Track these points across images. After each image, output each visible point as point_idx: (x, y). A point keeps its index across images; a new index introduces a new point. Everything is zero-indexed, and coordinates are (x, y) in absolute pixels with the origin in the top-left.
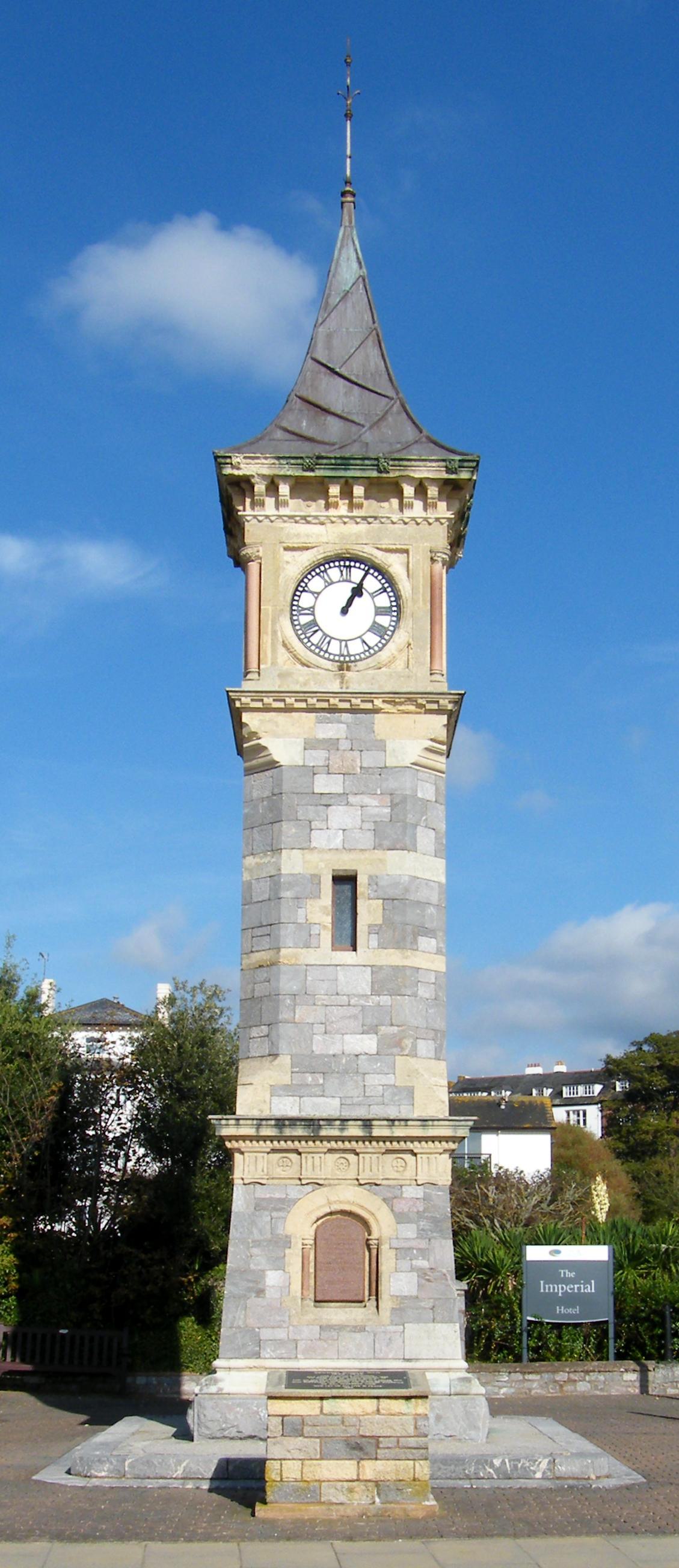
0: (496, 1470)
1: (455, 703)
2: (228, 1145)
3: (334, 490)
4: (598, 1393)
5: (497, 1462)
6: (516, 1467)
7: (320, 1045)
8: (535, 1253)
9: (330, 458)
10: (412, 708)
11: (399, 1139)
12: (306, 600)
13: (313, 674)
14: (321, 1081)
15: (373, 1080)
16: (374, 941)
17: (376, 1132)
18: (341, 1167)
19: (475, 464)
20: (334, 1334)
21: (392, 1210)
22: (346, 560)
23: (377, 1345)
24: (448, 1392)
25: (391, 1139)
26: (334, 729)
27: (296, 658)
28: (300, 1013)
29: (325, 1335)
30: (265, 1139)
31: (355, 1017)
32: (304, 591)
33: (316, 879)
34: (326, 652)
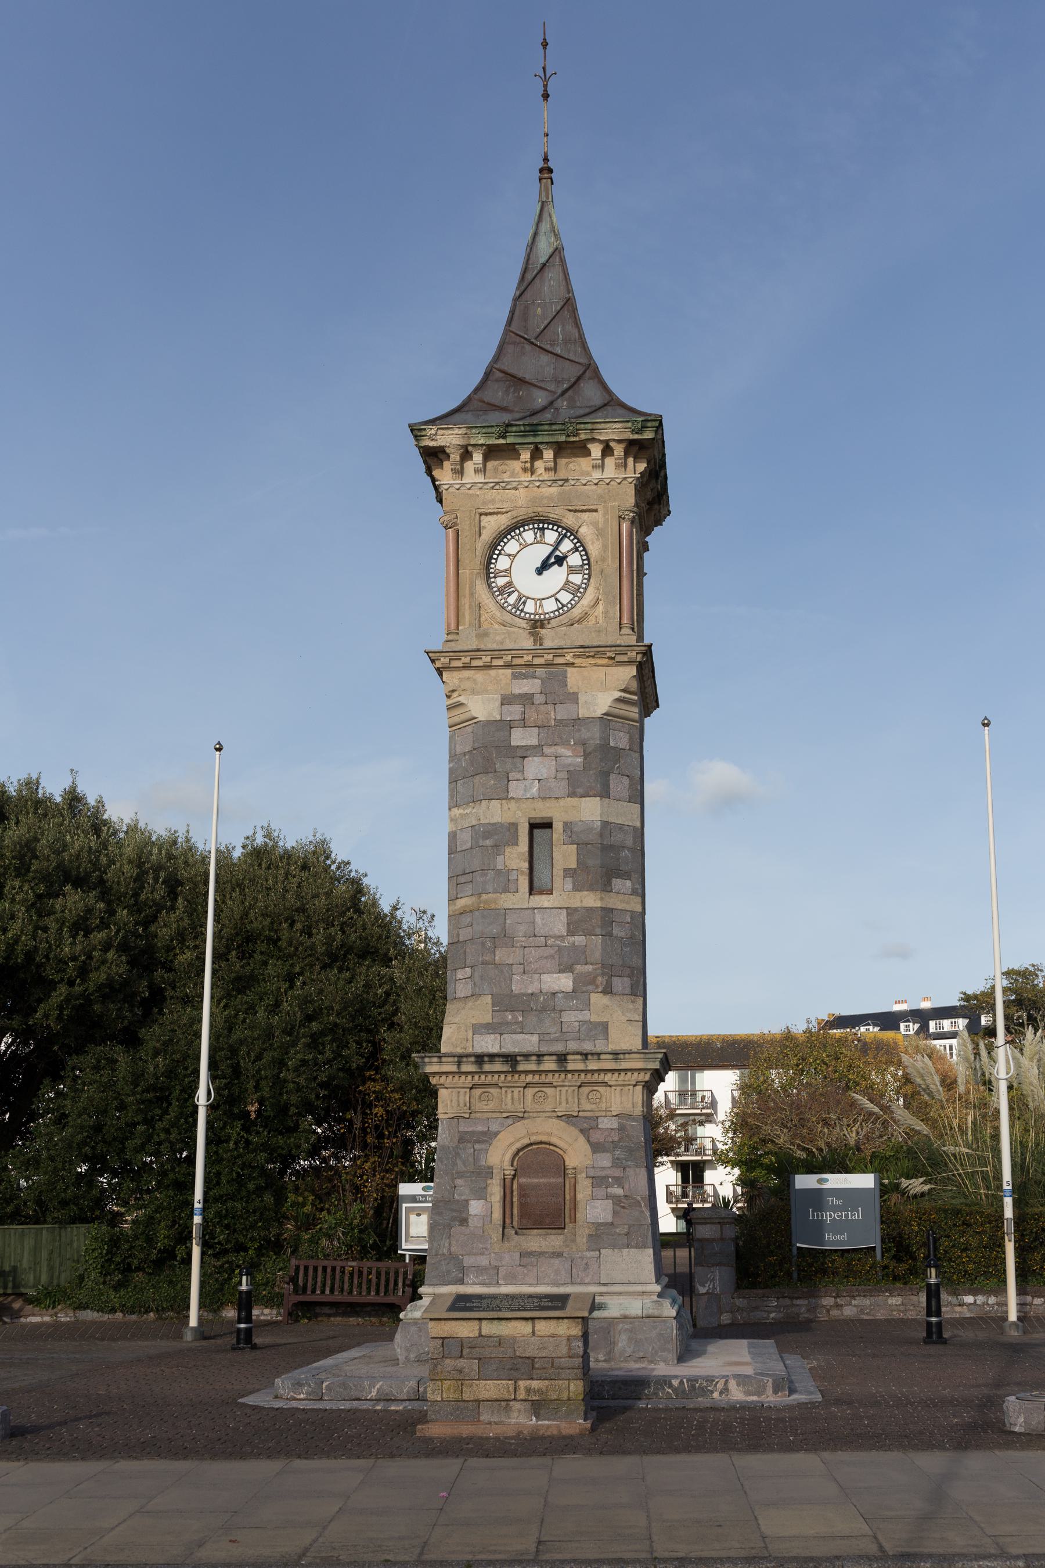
0: (675, 1390)
4: (865, 1317)
5: (675, 1383)
6: (693, 1386)
7: (518, 985)
8: (804, 1181)
10: (605, 661)
12: (502, 563)
13: (509, 633)
14: (520, 1019)
15: (569, 1017)
17: (571, 1066)
21: (588, 1141)
23: (574, 1270)
25: (586, 1071)
26: (528, 686)
29: (525, 1260)
33: (514, 826)
34: (522, 611)
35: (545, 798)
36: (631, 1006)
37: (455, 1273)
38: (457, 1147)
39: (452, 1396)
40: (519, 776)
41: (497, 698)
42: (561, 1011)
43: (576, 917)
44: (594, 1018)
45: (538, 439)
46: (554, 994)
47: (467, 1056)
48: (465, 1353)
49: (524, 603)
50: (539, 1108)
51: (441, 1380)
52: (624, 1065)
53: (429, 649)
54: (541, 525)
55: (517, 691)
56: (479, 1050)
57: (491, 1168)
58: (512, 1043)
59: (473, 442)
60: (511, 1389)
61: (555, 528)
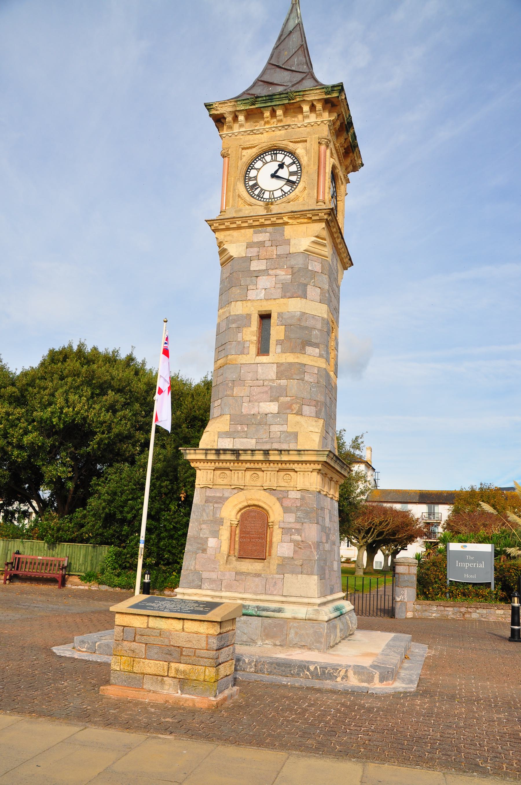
0: (311, 673)
1: (329, 214)
2: (192, 465)
3: (267, 114)
5: (312, 668)
9: (263, 97)
10: (306, 220)
11: (286, 462)
12: (253, 173)
14: (246, 429)
16: (279, 349)
17: (272, 458)
18: (255, 479)
19: (340, 88)
20: (243, 577)
21: (282, 505)
22: (274, 150)
23: (267, 586)
24: (304, 618)
25: (282, 462)
26: (263, 237)
27: (245, 202)
28: (236, 391)
29: (238, 577)
30: (211, 461)
31: (266, 392)
32: (252, 169)
33: (249, 316)
35: (268, 299)
36: (314, 423)
37: (197, 582)
38: (204, 505)
39: (127, 668)
40: (254, 288)
41: (245, 244)
42: (270, 425)
43: (282, 368)
44: (290, 430)
45: (273, 104)
46: (266, 414)
47: (210, 450)
48: (136, 639)
49: (264, 193)
50: (253, 483)
51: (121, 656)
52: (304, 458)
53: (207, 219)
54: (275, 152)
55: (256, 240)
56: (220, 447)
57: (222, 519)
58: (239, 444)
59: (238, 109)
60: (166, 668)
61: (283, 152)
